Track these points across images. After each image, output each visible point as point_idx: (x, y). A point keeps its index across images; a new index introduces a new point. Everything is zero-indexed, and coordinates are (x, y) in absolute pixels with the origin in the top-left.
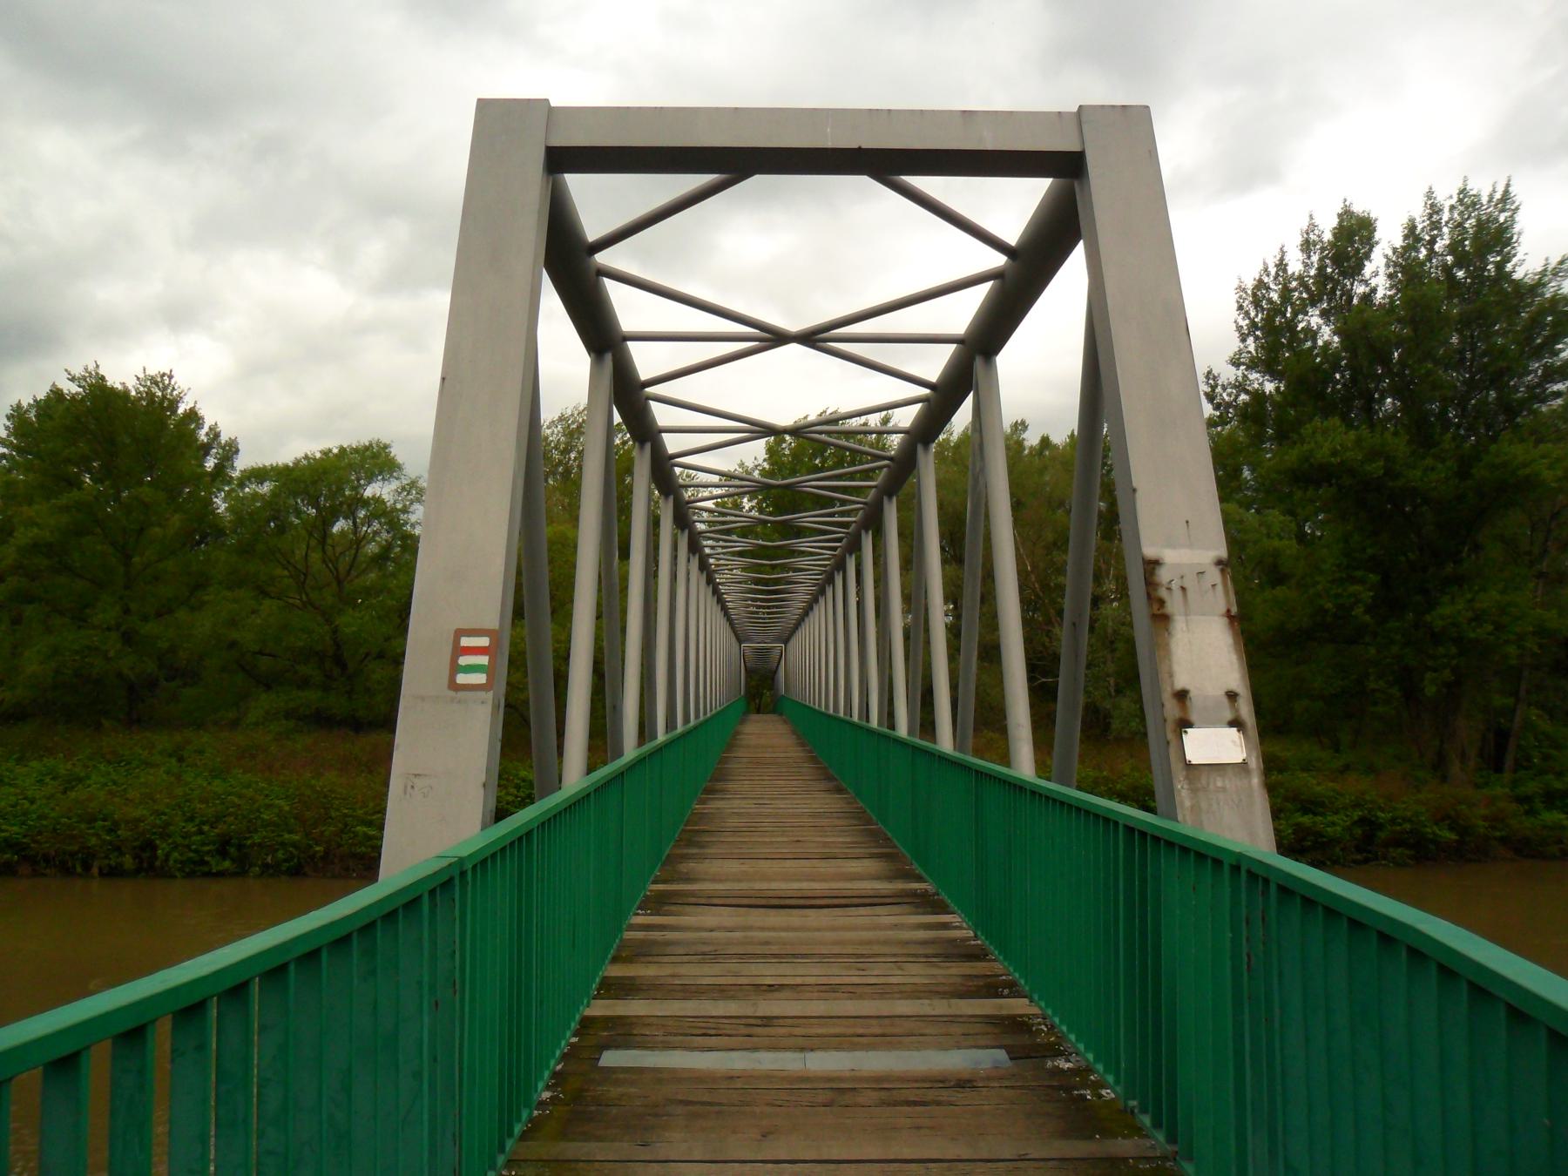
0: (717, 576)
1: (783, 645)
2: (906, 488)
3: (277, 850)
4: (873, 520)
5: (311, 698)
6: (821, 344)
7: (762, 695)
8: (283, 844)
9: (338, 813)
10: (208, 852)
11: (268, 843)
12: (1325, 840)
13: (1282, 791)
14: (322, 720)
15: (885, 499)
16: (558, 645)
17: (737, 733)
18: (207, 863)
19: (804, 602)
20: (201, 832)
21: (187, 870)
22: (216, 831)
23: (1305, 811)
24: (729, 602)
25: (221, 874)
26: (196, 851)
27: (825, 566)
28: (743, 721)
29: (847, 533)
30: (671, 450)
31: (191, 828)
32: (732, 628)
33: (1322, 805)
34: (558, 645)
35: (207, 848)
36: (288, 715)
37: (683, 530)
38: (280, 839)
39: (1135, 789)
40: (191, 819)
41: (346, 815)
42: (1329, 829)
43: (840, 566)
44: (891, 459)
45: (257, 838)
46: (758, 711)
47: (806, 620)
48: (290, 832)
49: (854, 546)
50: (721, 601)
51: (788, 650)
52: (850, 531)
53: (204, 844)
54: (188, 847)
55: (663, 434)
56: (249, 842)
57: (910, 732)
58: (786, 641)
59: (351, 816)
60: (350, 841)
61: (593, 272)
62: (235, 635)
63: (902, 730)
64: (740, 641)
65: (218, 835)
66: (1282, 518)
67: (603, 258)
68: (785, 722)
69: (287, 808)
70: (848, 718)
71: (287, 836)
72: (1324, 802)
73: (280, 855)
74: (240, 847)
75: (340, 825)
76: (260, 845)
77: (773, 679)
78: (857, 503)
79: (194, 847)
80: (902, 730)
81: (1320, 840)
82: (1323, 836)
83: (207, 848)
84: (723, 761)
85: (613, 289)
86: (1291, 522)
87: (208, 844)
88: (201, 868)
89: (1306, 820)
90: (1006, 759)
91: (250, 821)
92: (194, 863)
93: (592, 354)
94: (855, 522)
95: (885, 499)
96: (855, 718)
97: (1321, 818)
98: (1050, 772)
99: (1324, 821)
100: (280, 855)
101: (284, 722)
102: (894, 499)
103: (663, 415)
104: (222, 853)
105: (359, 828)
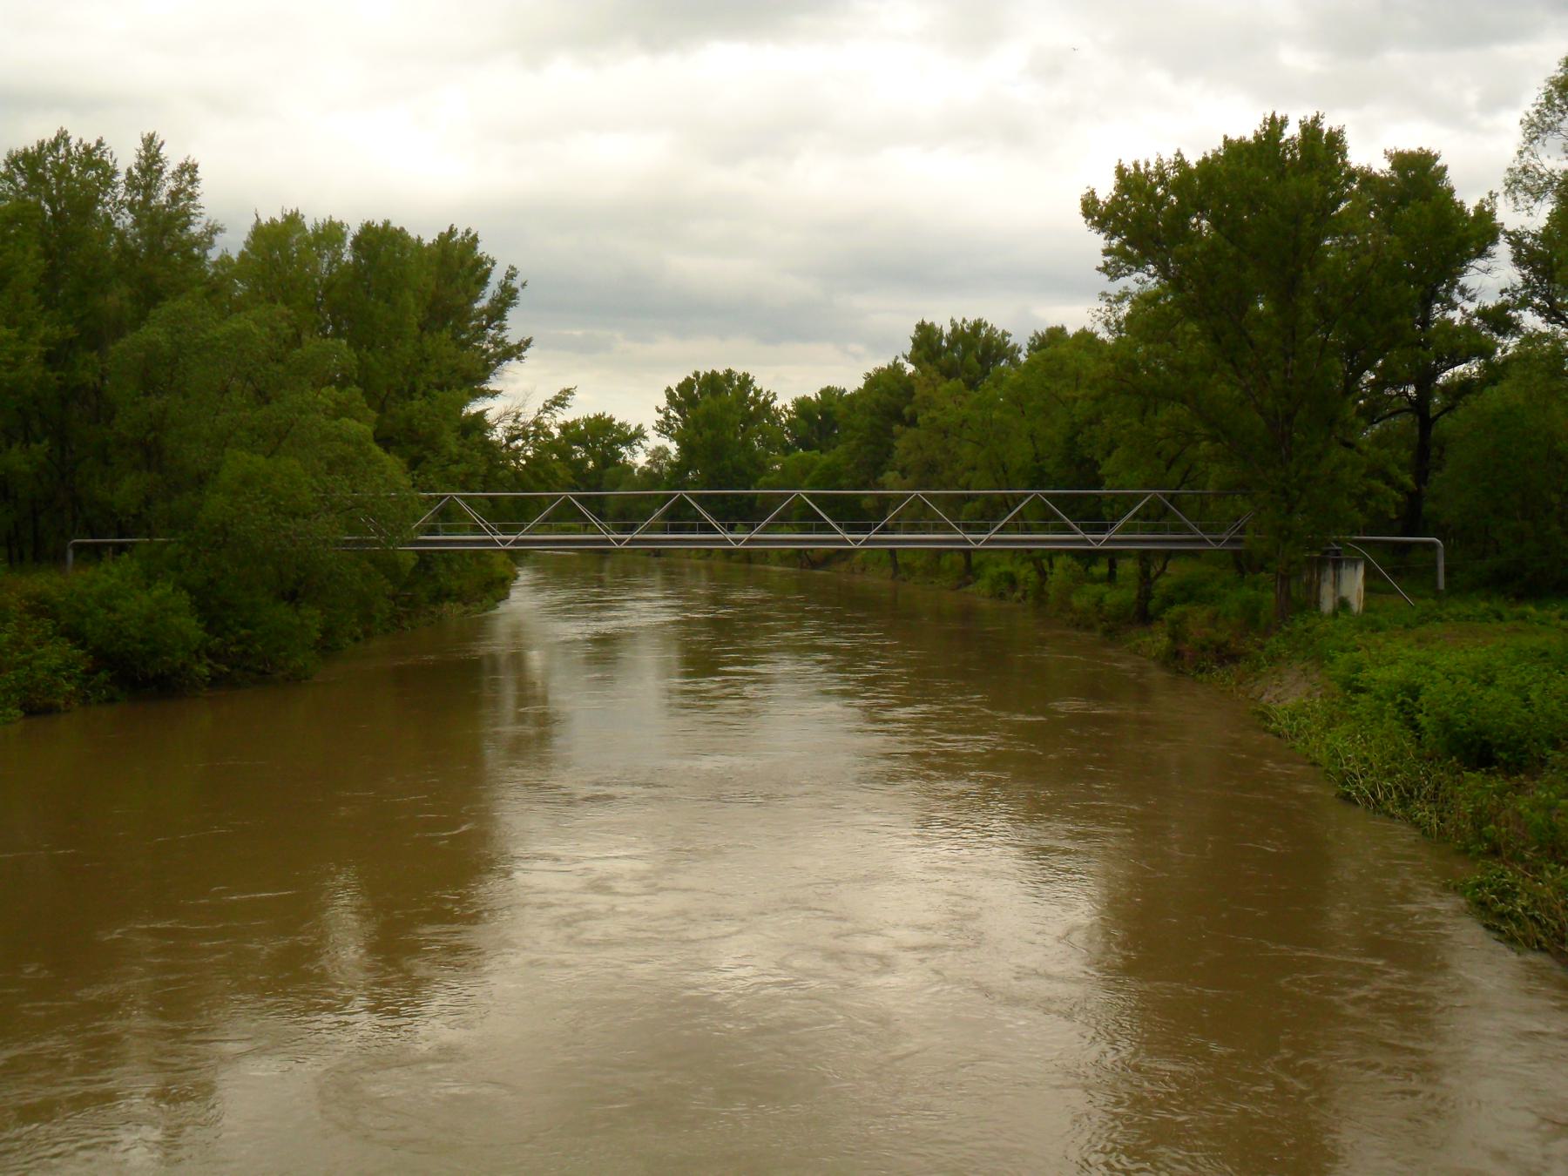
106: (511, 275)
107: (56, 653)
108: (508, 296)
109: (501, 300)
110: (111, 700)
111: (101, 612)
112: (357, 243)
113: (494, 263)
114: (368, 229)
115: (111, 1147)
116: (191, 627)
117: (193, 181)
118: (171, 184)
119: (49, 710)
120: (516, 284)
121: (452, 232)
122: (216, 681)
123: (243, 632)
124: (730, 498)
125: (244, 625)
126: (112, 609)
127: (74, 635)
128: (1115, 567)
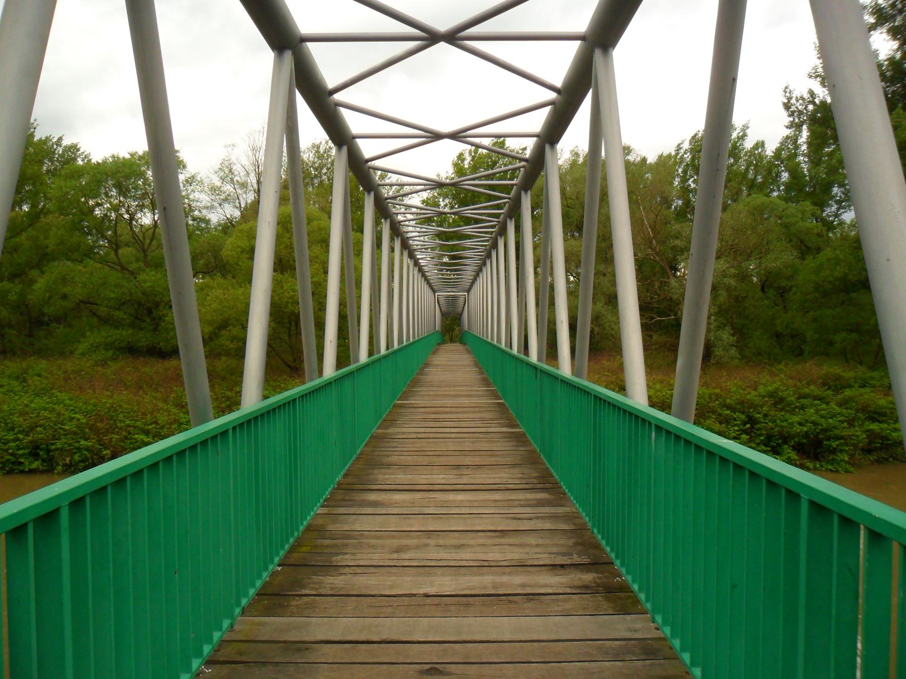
0: (417, 253)
1: (466, 294)
2: (539, 182)
3: (75, 453)
4: (515, 211)
5: (124, 334)
6: (464, 139)
7: (453, 330)
8: (79, 449)
9: (122, 424)
10: (23, 455)
11: (68, 448)
12: (891, 442)
13: (854, 404)
14: (132, 350)
15: (523, 193)
16: (294, 293)
17: (427, 365)
18: (21, 463)
19: (473, 272)
20: (17, 439)
21: (7, 469)
22: (29, 438)
23: (874, 420)
24: (427, 272)
25: (31, 471)
26: (12, 454)
27: (481, 255)
28: (434, 352)
29: (498, 222)
30: (367, 155)
31: (11, 436)
32: (431, 288)
33: (884, 415)
34: (294, 293)
35: (21, 452)
36: (107, 346)
37: (369, 192)
38: (77, 445)
39: (742, 403)
40: (13, 429)
41: (129, 426)
42: (893, 434)
43: (495, 246)
44: (526, 160)
45: (59, 445)
46: (452, 340)
47: (475, 282)
48: (86, 440)
49: (503, 231)
50: (423, 275)
51: (470, 298)
52: (500, 220)
53: (19, 449)
54: (7, 450)
55: (308, 44)
56: (53, 447)
57: (539, 359)
58: (468, 291)
59: (132, 427)
60: (131, 446)
61: (367, 169)
62: (67, 290)
63: (534, 357)
64: (434, 291)
65: (31, 442)
66: (811, 207)
67: (338, 97)
68: (469, 352)
69: (84, 421)
70: (508, 350)
71: (83, 442)
72: (886, 412)
73: (76, 457)
74: (48, 451)
75: (124, 433)
76: (61, 449)
77: (460, 319)
78: (505, 199)
79: (10, 451)
80: (534, 357)
81: (885, 442)
82: (888, 439)
83: (21, 452)
84: (377, 439)
85: (345, 113)
86: (817, 210)
87: (21, 449)
88: (19, 467)
89: (874, 427)
90: (557, 366)
91: (56, 431)
92: (13, 463)
93: (275, 51)
94: (516, 185)
95: (523, 193)
96: (515, 351)
97: (886, 425)
98: (672, 390)
99: (889, 427)
100: (76, 457)
101: (103, 352)
102: (529, 192)
103: (354, 123)
104: (34, 455)
105: (136, 436)
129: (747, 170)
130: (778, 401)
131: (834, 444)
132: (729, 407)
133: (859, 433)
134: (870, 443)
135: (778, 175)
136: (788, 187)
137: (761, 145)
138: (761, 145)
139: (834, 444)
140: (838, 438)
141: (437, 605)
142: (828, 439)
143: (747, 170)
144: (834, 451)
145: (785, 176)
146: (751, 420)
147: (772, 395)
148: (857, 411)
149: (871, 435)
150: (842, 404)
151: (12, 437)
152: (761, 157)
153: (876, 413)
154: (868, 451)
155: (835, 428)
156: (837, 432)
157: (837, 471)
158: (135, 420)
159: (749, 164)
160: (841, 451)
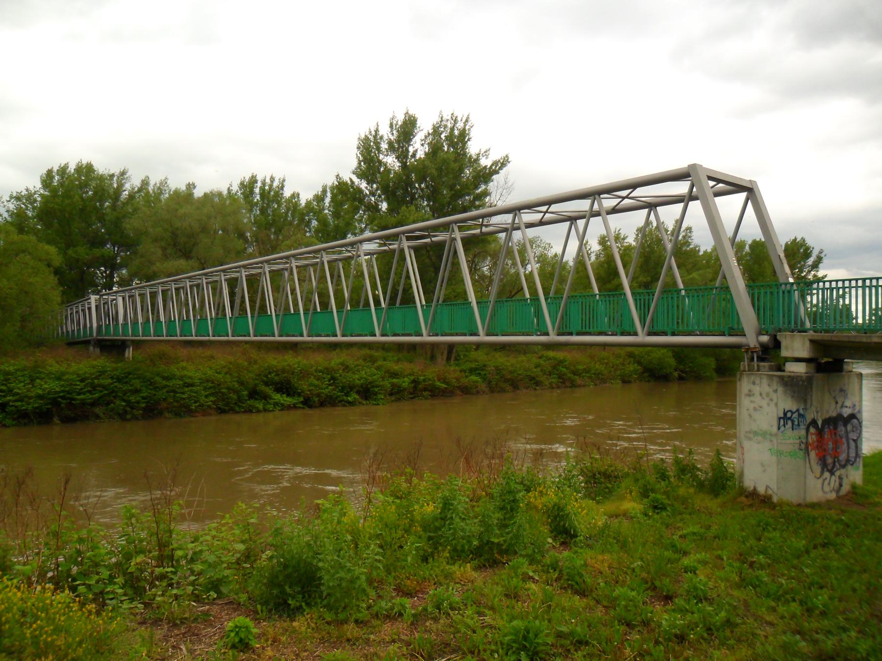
39: (327, 369)
89: (395, 380)
106: (821, 252)
107: (632, 367)
108: (819, 260)
109: (816, 261)
110: (649, 381)
111: (646, 356)
112: (750, 246)
113: (813, 248)
114: (754, 241)
115: (193, 540)
116: (672, 362)
117: (690, 232)
118: (684, 234)
119: (629, 382)
120: (822, 255)
121: (796, 239)
122: (681, 378)
123: (691, 365)
124: (536, 348)
125: (691, 363)
126: (650, 356)
127: (639, 363)
128: (39, 423)
129: (287, 213)
130: (346, 368)
131: (376, 390)
132: (320, 371)
133: (387, 383)
134: (392, 389)
135: (309, 221)
136: (317, 231)
137: (296, 196)
138: (296, 196)
139: (376, 390)
140: (377, 386)
141: (67, 482)
142: (373, 387)
143: (287, 213)
144: (376, 394)
145: (314, 223)
146: (333, 378)
147: (342, 364)
148: (385, 372)
149: (393, 385)
150: (378, 368)
151: (622, 443)
152: (296, 205)
153: (394, 374)
154: (391, 394)
155: (376, 381)
156: (377, 383)
157: (378, 404)
158: (676, 550)
159: (288, 209)
160: (380, 393)
